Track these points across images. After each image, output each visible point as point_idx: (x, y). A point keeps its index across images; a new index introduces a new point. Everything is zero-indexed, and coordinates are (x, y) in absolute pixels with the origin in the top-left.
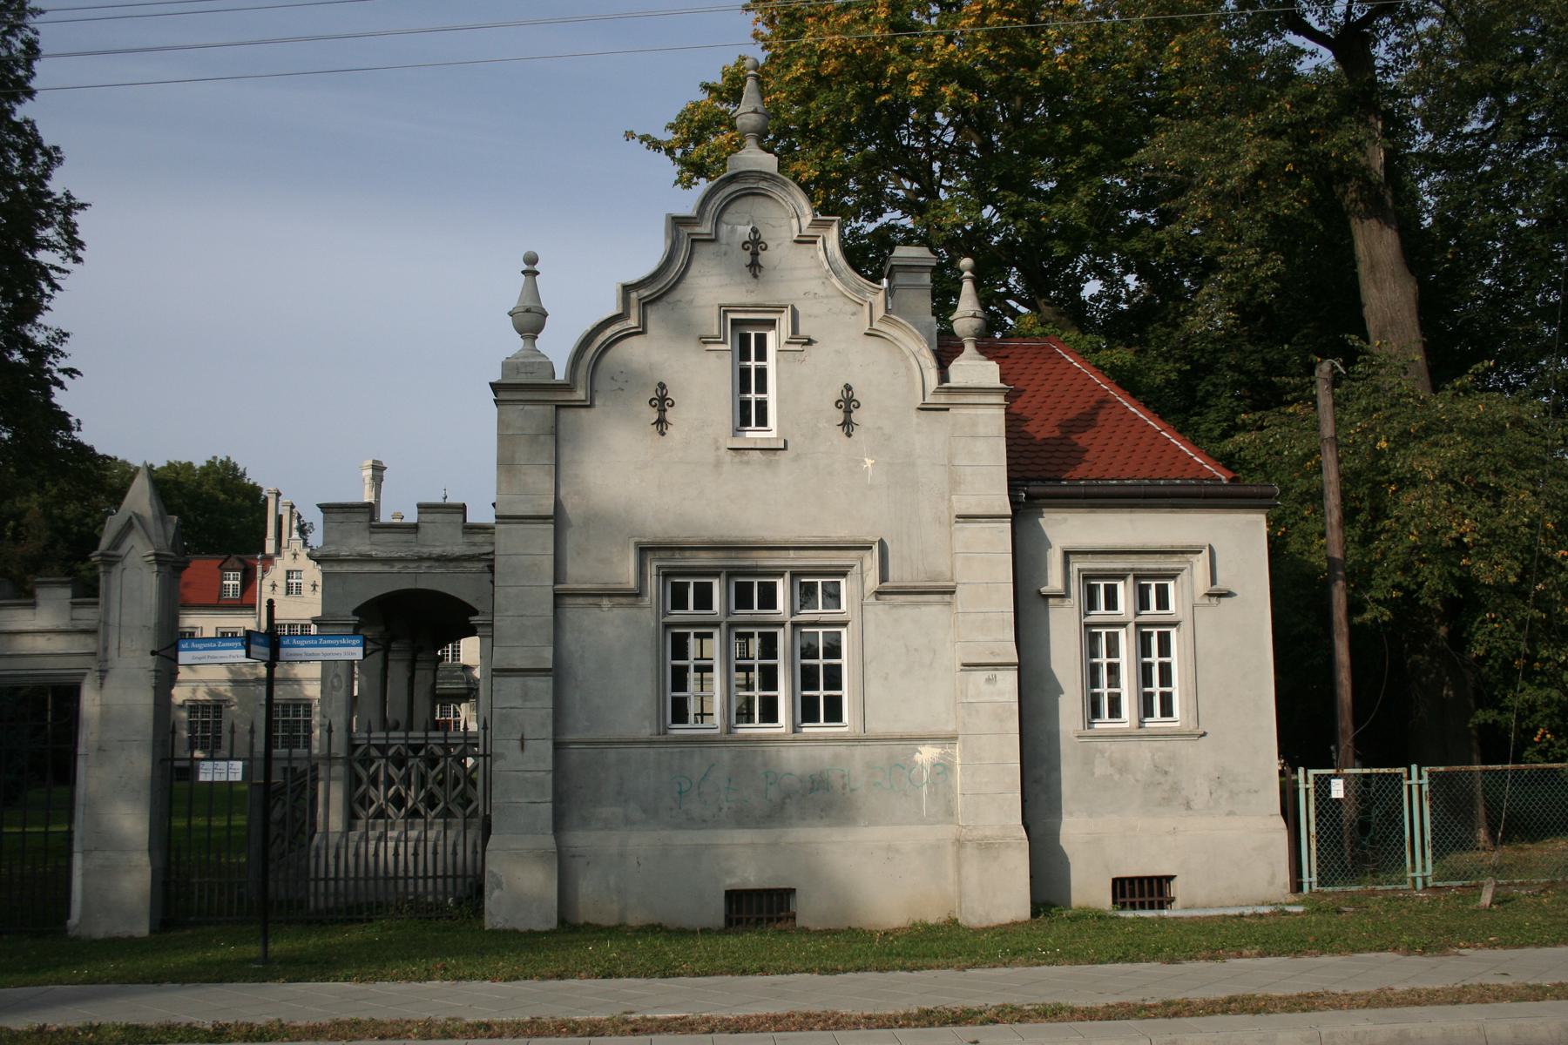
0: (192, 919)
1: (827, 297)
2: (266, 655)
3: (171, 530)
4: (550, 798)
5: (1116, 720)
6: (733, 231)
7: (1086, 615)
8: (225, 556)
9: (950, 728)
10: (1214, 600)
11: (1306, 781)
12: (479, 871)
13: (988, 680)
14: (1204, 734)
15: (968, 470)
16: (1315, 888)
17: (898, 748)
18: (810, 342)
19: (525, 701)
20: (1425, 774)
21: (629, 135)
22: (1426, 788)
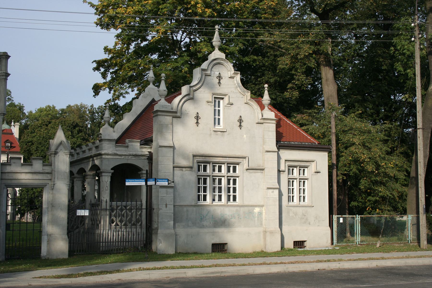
0: (75, 253)
1: (236, 93)
4: (173, 220)
6: (214, 73)
7: (227, 174)
9: (262, 204)
10: (316, 173)
12: (331, 216)
16: (336, 244)
18: (232, 104)
19: (167, 195)
20: (359, 217)
22: (359, 220)
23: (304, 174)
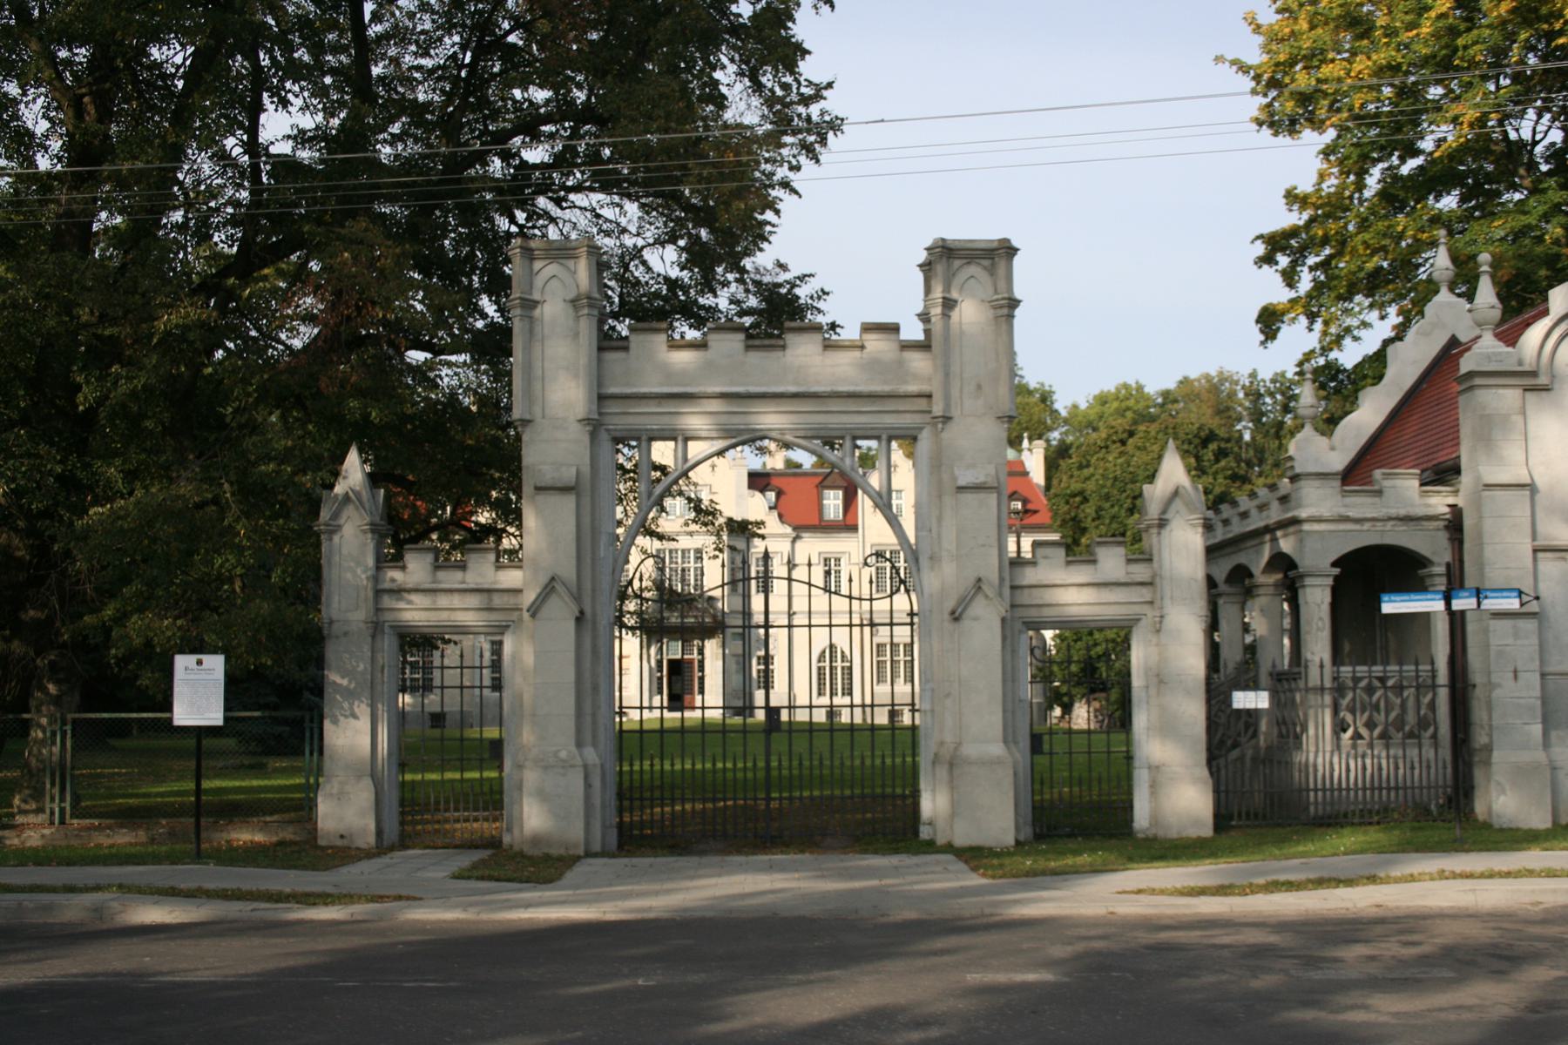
0: (1234, 823)
8: (860, 492)
21: (1219, 59)
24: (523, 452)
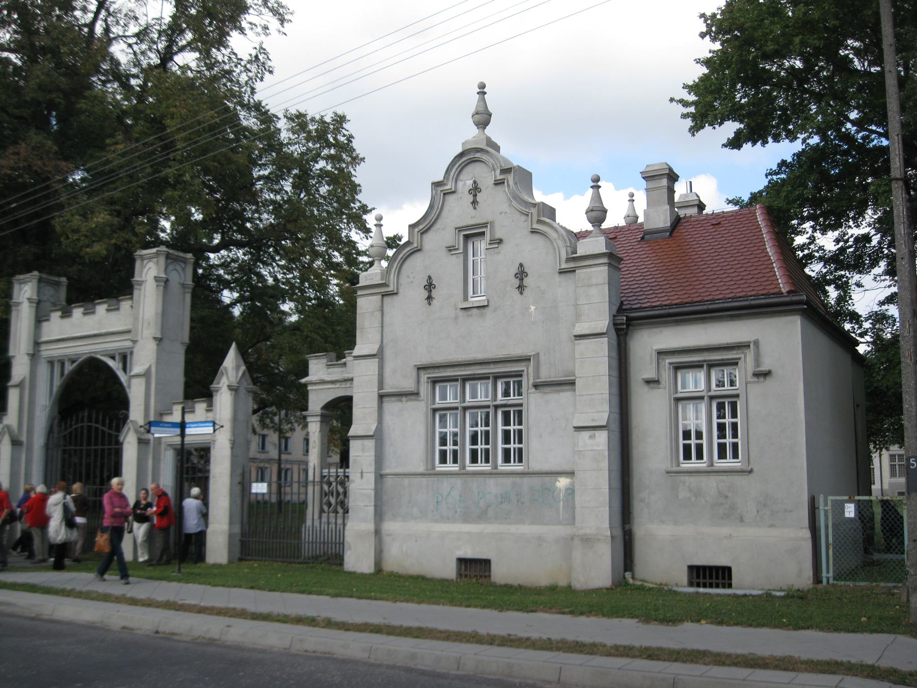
2: (697, 411)
3: (240, 373)
5: (699, 461)
6: (465, 184)
11: (826, 505)
13: (591, 437)
14: (751, 471)
15: (586, 307)
17: (547, 479)
20: (829, 503)
23: (684, 387)
24: (155, 356)
